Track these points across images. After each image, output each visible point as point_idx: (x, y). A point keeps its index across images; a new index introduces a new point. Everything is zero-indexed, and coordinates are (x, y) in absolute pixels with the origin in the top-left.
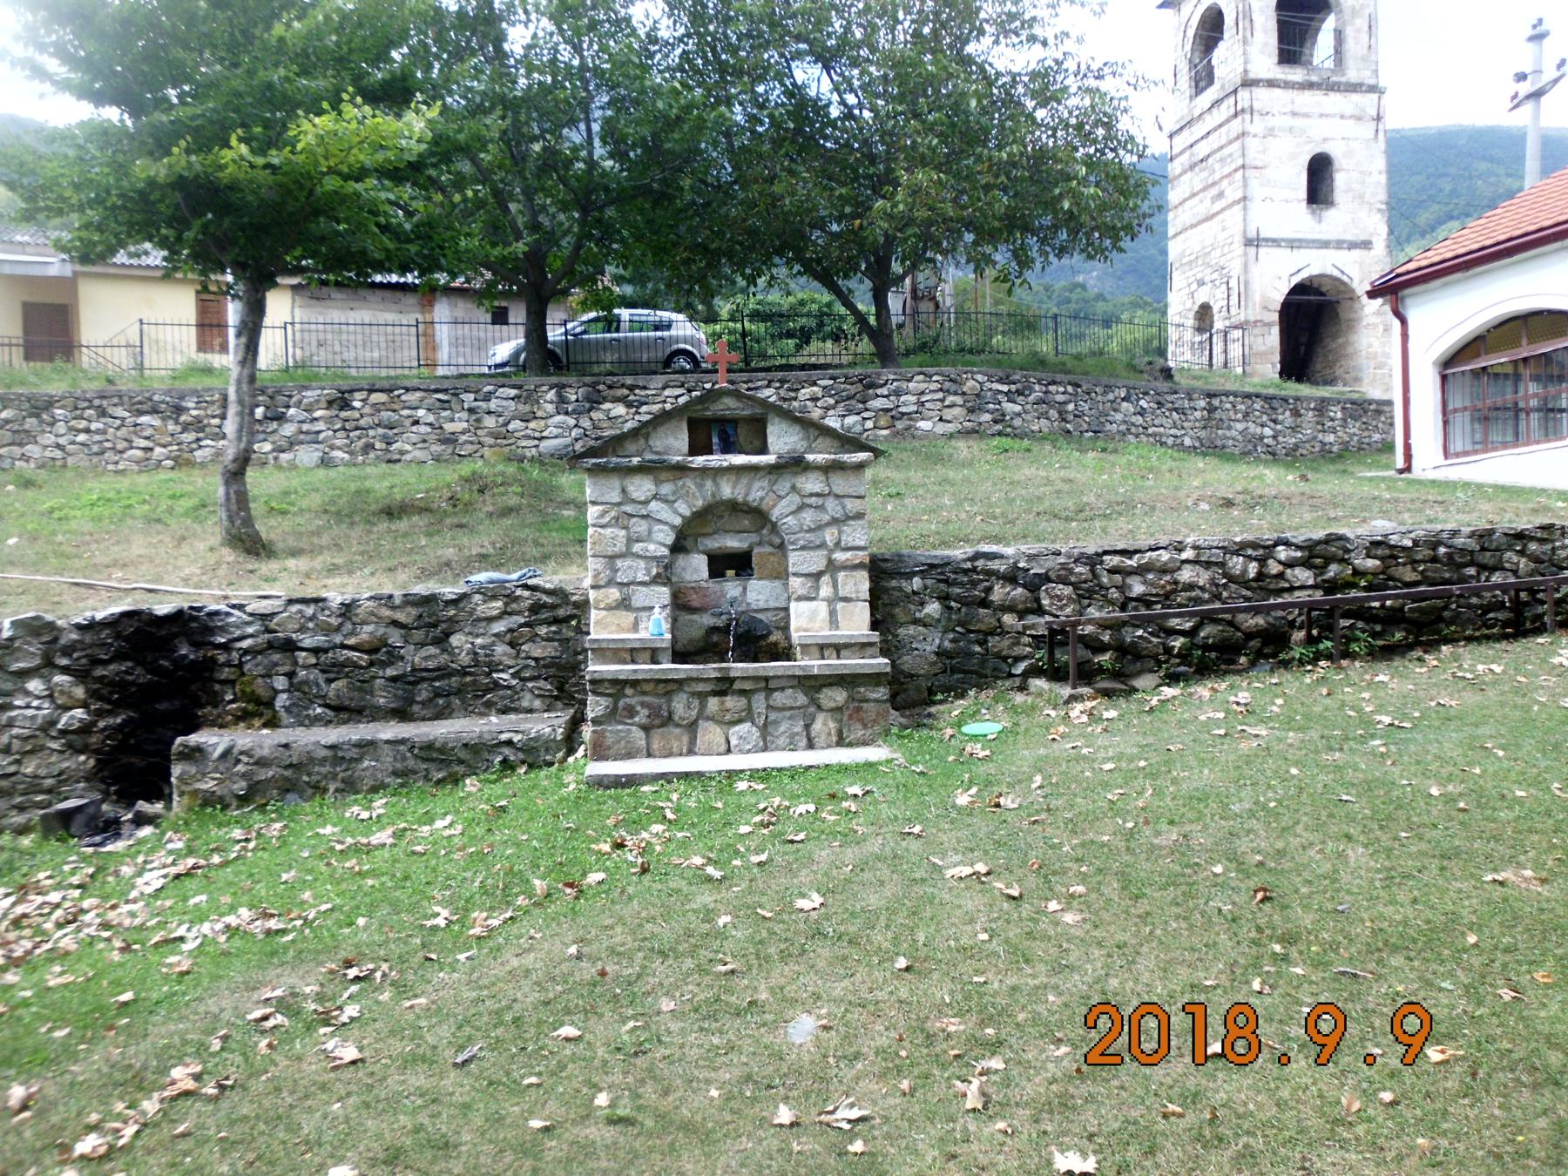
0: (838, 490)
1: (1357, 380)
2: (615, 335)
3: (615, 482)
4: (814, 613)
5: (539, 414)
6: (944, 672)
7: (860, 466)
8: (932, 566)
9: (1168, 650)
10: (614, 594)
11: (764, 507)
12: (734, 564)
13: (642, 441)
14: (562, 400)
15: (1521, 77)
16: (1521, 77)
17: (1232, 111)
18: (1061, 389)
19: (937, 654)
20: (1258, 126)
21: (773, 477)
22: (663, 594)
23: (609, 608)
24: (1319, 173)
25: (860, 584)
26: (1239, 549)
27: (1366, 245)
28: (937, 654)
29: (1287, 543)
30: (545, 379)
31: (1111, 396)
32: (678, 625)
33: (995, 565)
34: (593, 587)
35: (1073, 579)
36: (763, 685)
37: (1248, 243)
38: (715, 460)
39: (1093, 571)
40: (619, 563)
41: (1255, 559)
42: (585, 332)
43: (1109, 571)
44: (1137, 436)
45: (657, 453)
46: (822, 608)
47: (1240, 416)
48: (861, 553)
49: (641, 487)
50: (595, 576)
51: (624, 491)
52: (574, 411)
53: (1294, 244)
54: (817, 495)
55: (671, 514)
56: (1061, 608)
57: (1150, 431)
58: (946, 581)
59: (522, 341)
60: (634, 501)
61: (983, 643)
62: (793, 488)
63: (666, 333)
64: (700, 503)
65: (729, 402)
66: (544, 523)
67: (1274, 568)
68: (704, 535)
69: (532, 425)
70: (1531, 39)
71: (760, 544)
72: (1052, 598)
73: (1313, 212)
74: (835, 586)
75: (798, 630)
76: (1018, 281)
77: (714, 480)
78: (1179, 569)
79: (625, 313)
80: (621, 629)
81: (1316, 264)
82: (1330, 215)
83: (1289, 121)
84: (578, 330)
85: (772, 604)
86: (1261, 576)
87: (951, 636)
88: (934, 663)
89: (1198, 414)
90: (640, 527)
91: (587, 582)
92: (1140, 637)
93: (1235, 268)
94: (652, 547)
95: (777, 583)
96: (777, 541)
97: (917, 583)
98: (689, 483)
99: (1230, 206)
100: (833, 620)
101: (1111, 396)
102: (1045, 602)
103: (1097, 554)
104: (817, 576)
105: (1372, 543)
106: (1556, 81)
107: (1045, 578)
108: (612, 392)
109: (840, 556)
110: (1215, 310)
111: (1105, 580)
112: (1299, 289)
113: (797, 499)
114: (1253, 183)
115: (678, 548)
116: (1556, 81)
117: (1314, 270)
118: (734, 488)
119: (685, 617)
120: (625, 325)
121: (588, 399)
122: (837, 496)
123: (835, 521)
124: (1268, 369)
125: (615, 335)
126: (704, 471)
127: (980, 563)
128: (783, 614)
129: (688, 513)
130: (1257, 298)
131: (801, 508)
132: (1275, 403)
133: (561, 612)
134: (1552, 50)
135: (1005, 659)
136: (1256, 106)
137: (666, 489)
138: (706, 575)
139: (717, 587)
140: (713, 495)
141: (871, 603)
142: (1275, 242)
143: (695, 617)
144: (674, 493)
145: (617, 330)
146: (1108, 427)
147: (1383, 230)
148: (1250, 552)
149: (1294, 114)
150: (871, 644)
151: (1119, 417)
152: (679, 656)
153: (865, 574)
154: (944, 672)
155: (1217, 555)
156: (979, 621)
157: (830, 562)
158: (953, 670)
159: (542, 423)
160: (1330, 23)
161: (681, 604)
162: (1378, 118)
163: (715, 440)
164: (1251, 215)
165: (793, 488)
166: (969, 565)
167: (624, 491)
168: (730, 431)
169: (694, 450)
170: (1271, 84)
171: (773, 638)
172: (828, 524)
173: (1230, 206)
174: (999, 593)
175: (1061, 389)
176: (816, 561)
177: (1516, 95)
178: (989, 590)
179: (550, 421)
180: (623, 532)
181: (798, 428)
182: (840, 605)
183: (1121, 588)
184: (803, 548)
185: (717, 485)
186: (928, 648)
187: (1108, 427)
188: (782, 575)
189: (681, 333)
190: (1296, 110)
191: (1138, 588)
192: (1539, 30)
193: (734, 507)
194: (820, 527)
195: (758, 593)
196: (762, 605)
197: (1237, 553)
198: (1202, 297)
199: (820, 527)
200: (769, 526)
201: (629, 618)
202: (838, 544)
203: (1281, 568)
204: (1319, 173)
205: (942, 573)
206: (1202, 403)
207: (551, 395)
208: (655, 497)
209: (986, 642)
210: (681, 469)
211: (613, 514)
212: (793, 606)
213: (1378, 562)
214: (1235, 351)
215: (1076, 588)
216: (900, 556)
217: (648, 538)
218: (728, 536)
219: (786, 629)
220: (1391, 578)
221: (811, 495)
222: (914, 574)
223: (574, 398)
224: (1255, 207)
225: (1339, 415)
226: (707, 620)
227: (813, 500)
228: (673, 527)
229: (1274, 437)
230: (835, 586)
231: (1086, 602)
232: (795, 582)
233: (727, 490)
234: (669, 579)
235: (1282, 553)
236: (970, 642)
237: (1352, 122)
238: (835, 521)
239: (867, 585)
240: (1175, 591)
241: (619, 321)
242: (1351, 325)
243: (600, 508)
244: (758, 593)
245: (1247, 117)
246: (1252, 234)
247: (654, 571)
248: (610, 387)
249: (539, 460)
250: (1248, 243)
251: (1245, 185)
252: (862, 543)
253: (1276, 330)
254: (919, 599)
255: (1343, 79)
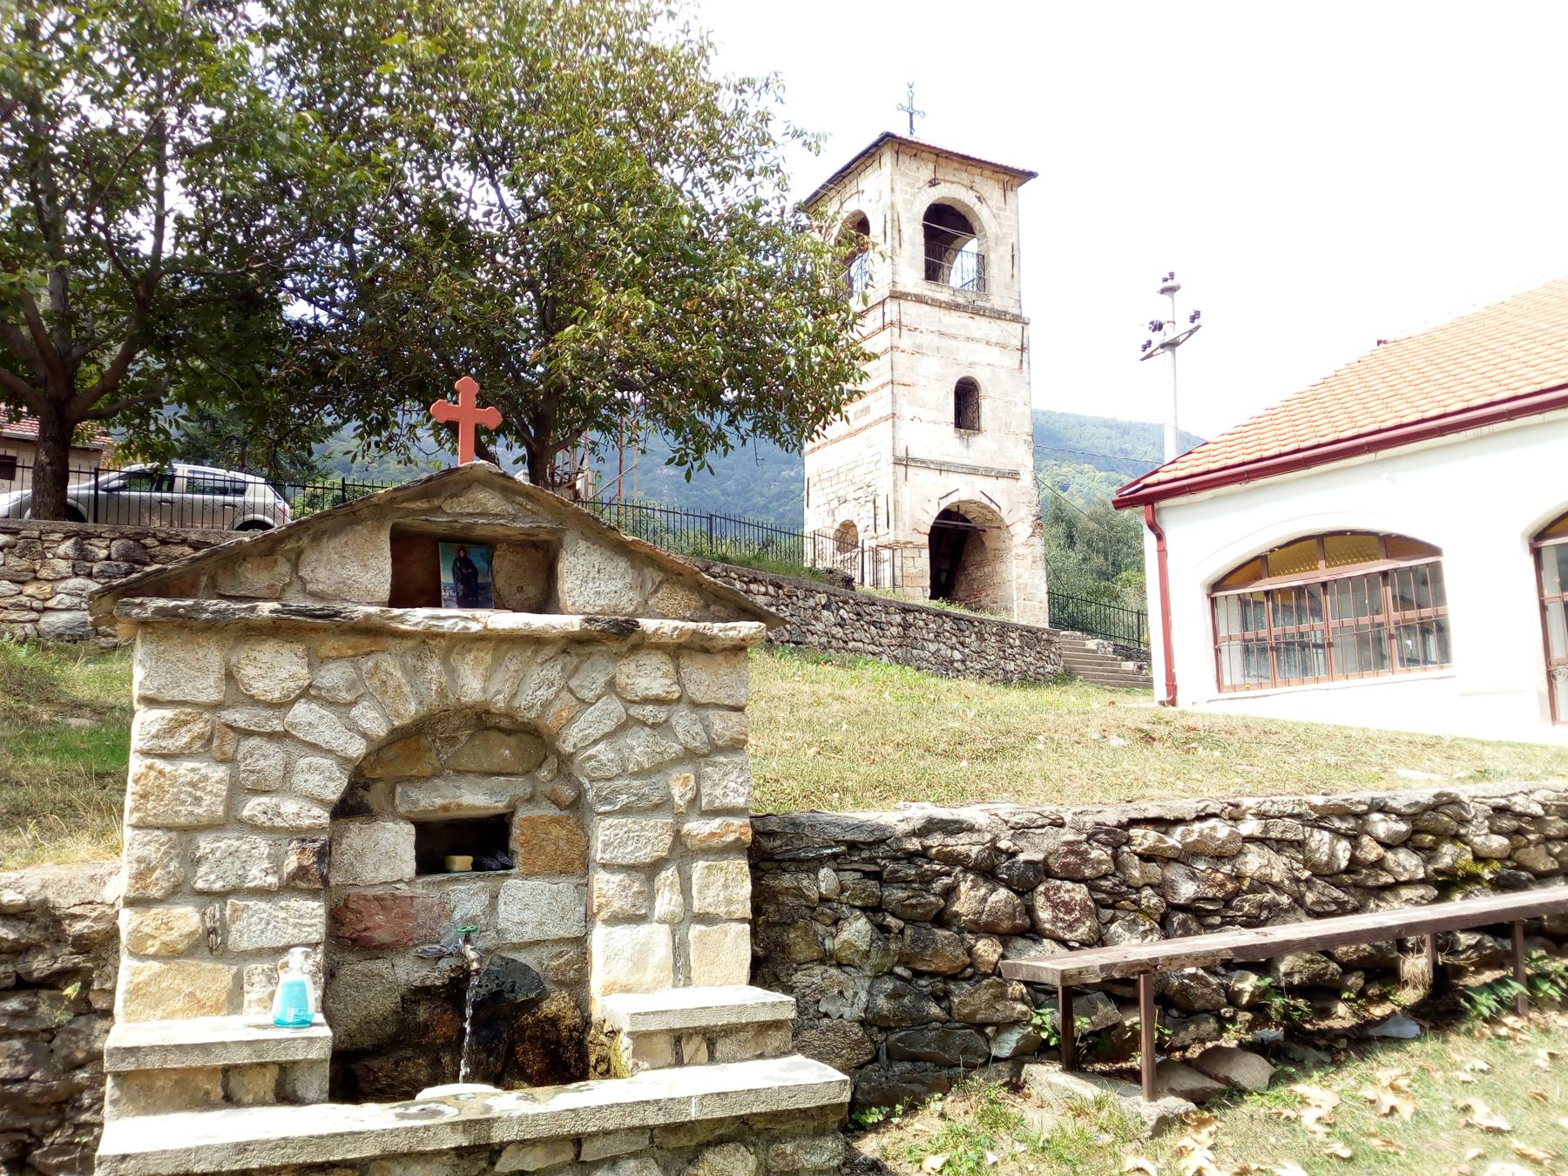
0: (697, 693)
1: (1008, 610)
2: (167, 495)
3: (212, 656)
4: (644, 950)
5: (43, 574)
6: (875, 1059)
7: (738, 649)
8: (853, 846)
9: (1233, 998)
10: (186, 918)
11: (550, 721)
12: (479, 843)
13: (284, 568)
14: (83, 555)
15: (1158, 327)
16: (1158, 327)
17: (880, 324)
18: (763, 589)
19: (863, 1023)
20: (906, 342)
21: (572, 660)
22: (310, 915)
23: (170, 954)
24: (966, 395)
25: (730, 886)
26: (1320, 818)
27: (1013, 475)
28: (863, 1023)
29: (1383, 809)
30: (58, 524)
31: (811, 602)
32: (339, 985)
33: (961, 844)
34: (131, 903)
35: (1088, 872)
36: (568, 1155)
37: (897, 462)
38: (452, 618)
39: (1115, 857)
40: (204, 844)
41: (1345, 836)
42: (123, 488)
43: (1141, 856)
44: (838, 650)
45: (314, 595)
46: (656, 936)
47: (932, 635)
48: (736, 822)
49: (274, 669)
50: (140, 876)
51: (230, 676)
52: (102, 573)
53: (942, 468)
54: (658, 701)
55: (340, 735)
56: (1071, 927)
57: (851, 644)
58: (876, 876)
59: (28, 491)
60: (254, 701)
61: (941, 998)
62: (611, 684)
63: (238, 499)
64: (410, 710)
65: (490, 501)
66: (28, 738)
67: (1371, 851)
68: (410, 780)
69: (30, 589)
70: (1163, 291)
71: (531, 800)
72: (1055, 906)
73: (961, 436)
74: (686, 891)
75: (609, 990)
76: (697, 464)
77: (445, 661)
78: (1240, 852)
79: (182, 469)
80: (198, 1006)
81: (966, 490)
82: (978, 441)
83: (936, 340)
84: (115, 484)
85: (554, 931)
86: (1355, 864)
87: (889, 985)
88: (858, 1043)
89: (894, 630)
90: (266, 759)
91: (118, 887)
92: (1193, 977)
93: (884, 487)
94: (290, 807)
95: (565, 886)
96: (568, 793)
97: (827, 880)
98: (390, 665)
99: (876, 422)
100: (681, 969)
101: (811, 602)
102: (1045, 915)
103: (1121, 826)
104: (652, 869)
105: (1495, 809)
106: (1191, 332)
107: (1042, 870)
108: (165, 550)
109: (698, 828)
110: (860, 528)
111: (1136, 873)
112: (946, 514)
113: (613, 709)
114: (902, 401)
115: (349, 809)
116: (1191, 332)
117: (964, 495)
118: (487, 679)
119: (355, 967)
120: (180, 483)
121: (126, 556)
122: (695, 705)
123: (690, 756)
124: (919, 594)
125: (167, 495)
126: (426, 638)
127: (935, 841)
128: (572, 953)
129: (379, 729)
130: (906, 518)
131: (623, 727)
132: (963, 625)
133: (40, 965)
134: (1183, 305)
135: (980, 1027)
136: (904, 322)
137: (334, 676)
138: (410, 867)
139: (435, 893)
140: (442, 693)
141: (753, 923)
142: (925, 464)
143: (380, 966)
144: (351, 686)
145: (170, 489)
146: (810, 638)
147: (1030, 462)
148: (1337, 824)
149: (942, 334)
150: (777, 1025)
151: (819, 627)
152: (351, 1078)
153: (743, 864)
154: (875, 1059)
155: (1295, 831)
156: (936, 953)
157: (678, 837)
158: (894, 1056)
159: (47, 588)
160: (972, 246)
161: (348, 938)
162: (1022, 349)
163: (447, 578)
164: (900, 434)
165: (611, 684)
166: (914, 844)
167: (230, 676)
168: (479, 563)
169: (402, 596)
170: (919, 299)
171: (549, 1008)
172: (678, 761)
173: (876, 422)
174: (970, 899)
175: (763, 589)
176: (650, 837)
177: (1149, 343)
178: (950, 892)
179: (61, 586)
180: (219, 773)
181: (623, 564)
182: (696, 930)
183: (1161, 888)
184: (626, 811)
185: (452, 672)
186: (847, 1012)
187: (810, 638)
188: (577, 865)
189: (260, 500)
190: (943, 330)
191: (1187, 891)
192: (1170, 283)
193: (482, 720)
194: (660, 768)
195: (522, 908)
196: (530, 933)
197: (1316, 824)
198: (843, 515)
199: (660, 768)
200: (553, 762)
201: (215, 977)
202: (694, 801)
203: (1381, 850)
204: (966, 395)
205: (872, 860)
206: (898, 619)
207: (67, 547)
208: (305, 693)
209: (947, 994)
210: (372, 632)
211: (198, 727)
212: (600, 937)
213: (1505, 841)
214: (886, 572)
215: (1093, 888)
216: (795, 824)
217: (284, 785)
218: (463, 782)
219: (578, 984)
220: (1520, 867)
221: (646, 701)
222: (821, 861)
223: (103, 553)
224: (905, 427)
225: (1017, 642)
226: (407, 971)
227: (648, 712)
228: (344, 761)
229: (963, 662)
230: (686, 891)
231: (1108, 913)
232: (605, 885)
233: (474, 683)
234: (325, 880)
235: (1382, 826)
236: (921, 996)
237: (996, 350)
238: (690, 756)
239: (746, 888)
240: (1237, 893)
241: (173, 478)
242: (999, 555)
243: (169, 713)
244: (522, 908)
245: (896, 330)
246: (901, 454)
247: (291, 864)
248: (164, 542)
249: (38, 642)
250: (897, 462)
251: (894, 403)
252: (740, 801)
253: (926, 553)
254: (828, 911)
255: (988, 305)
